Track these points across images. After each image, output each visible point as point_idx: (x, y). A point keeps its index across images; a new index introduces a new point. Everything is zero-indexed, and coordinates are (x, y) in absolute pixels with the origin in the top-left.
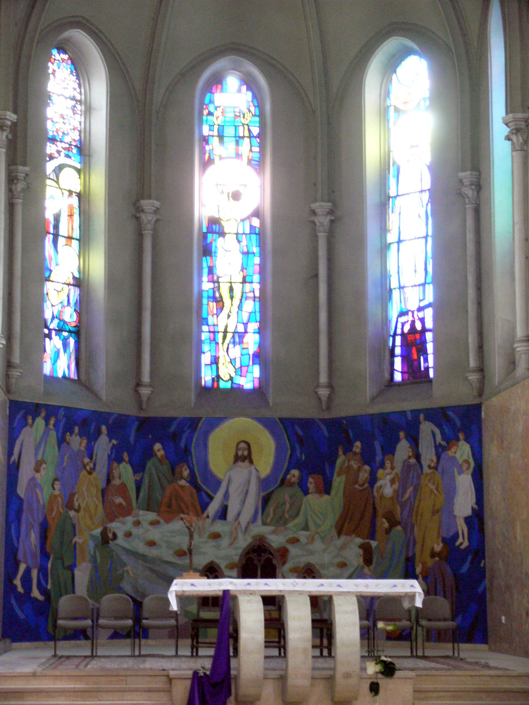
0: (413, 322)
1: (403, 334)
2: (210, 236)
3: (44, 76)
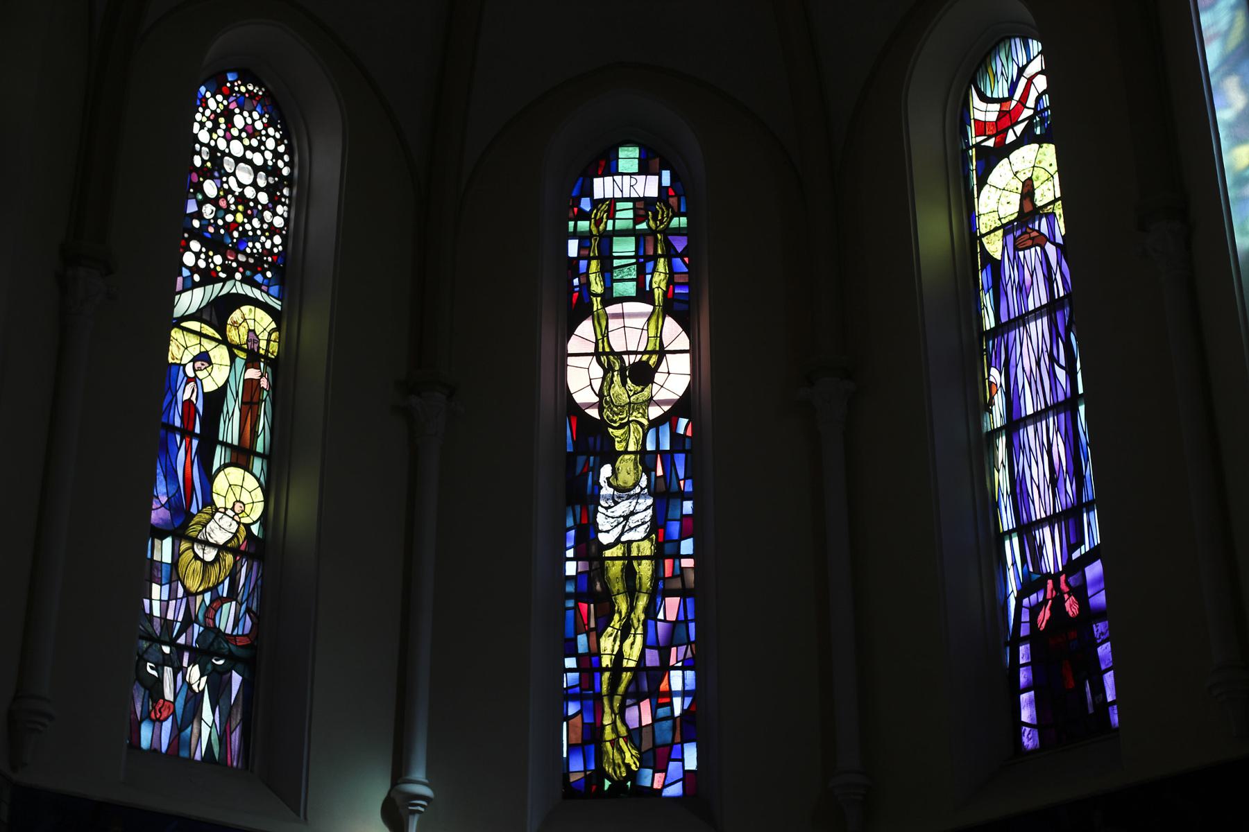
0: (1058, 604)
1: (1035, 638)
2: (581, 460)
3: (189, 542)
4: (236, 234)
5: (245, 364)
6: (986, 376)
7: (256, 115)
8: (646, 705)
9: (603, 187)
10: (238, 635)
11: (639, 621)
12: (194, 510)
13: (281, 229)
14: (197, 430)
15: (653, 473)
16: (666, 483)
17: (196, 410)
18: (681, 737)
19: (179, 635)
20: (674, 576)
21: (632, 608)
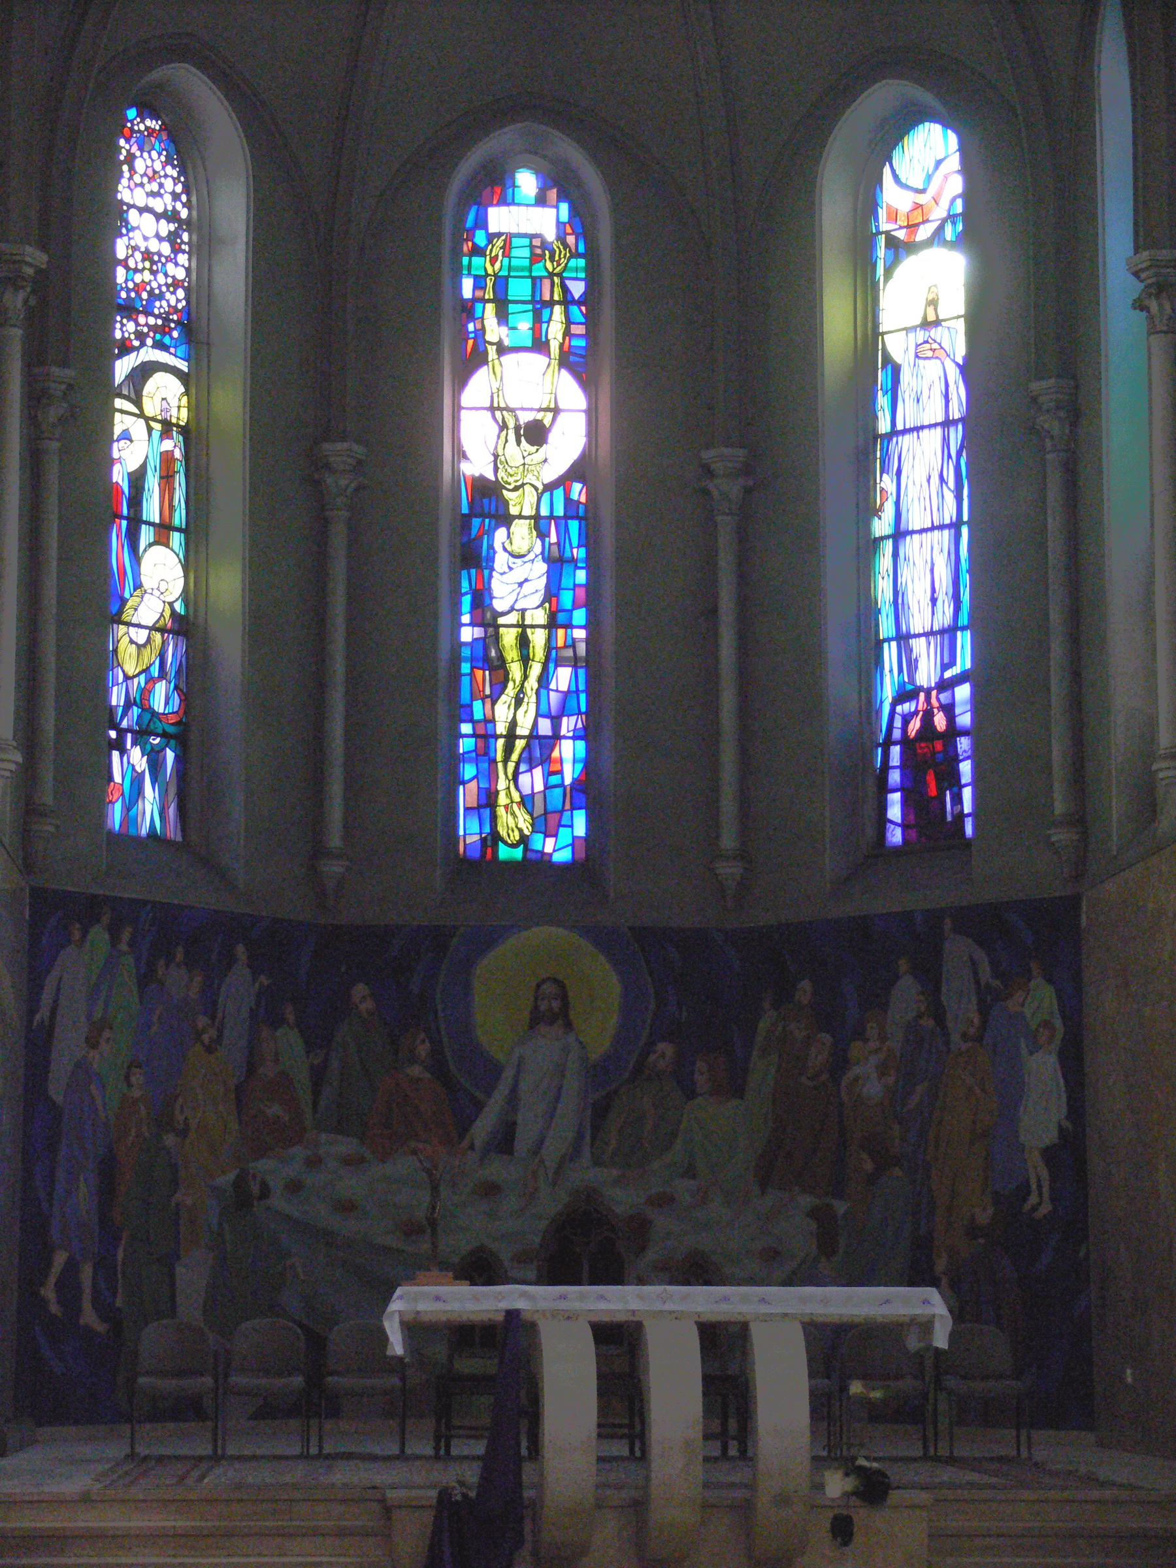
1: (905, 742)
2: (476, 522)
4: (145, 295)
5: (161, 436)
6: (878, 481)
7: (154, 154)
8: (538, 772)
9: (499, 219)
10: (169, 713)
11: (532, 690)
12: (127, 595)
13: (184, 281)
14: (125, 512)
15: (547, 539)
16: (559, 549)
17: (123, 493)
18: (571, 803)
19: (122, 719)
20: (565, 647)
21: (525, 677)
